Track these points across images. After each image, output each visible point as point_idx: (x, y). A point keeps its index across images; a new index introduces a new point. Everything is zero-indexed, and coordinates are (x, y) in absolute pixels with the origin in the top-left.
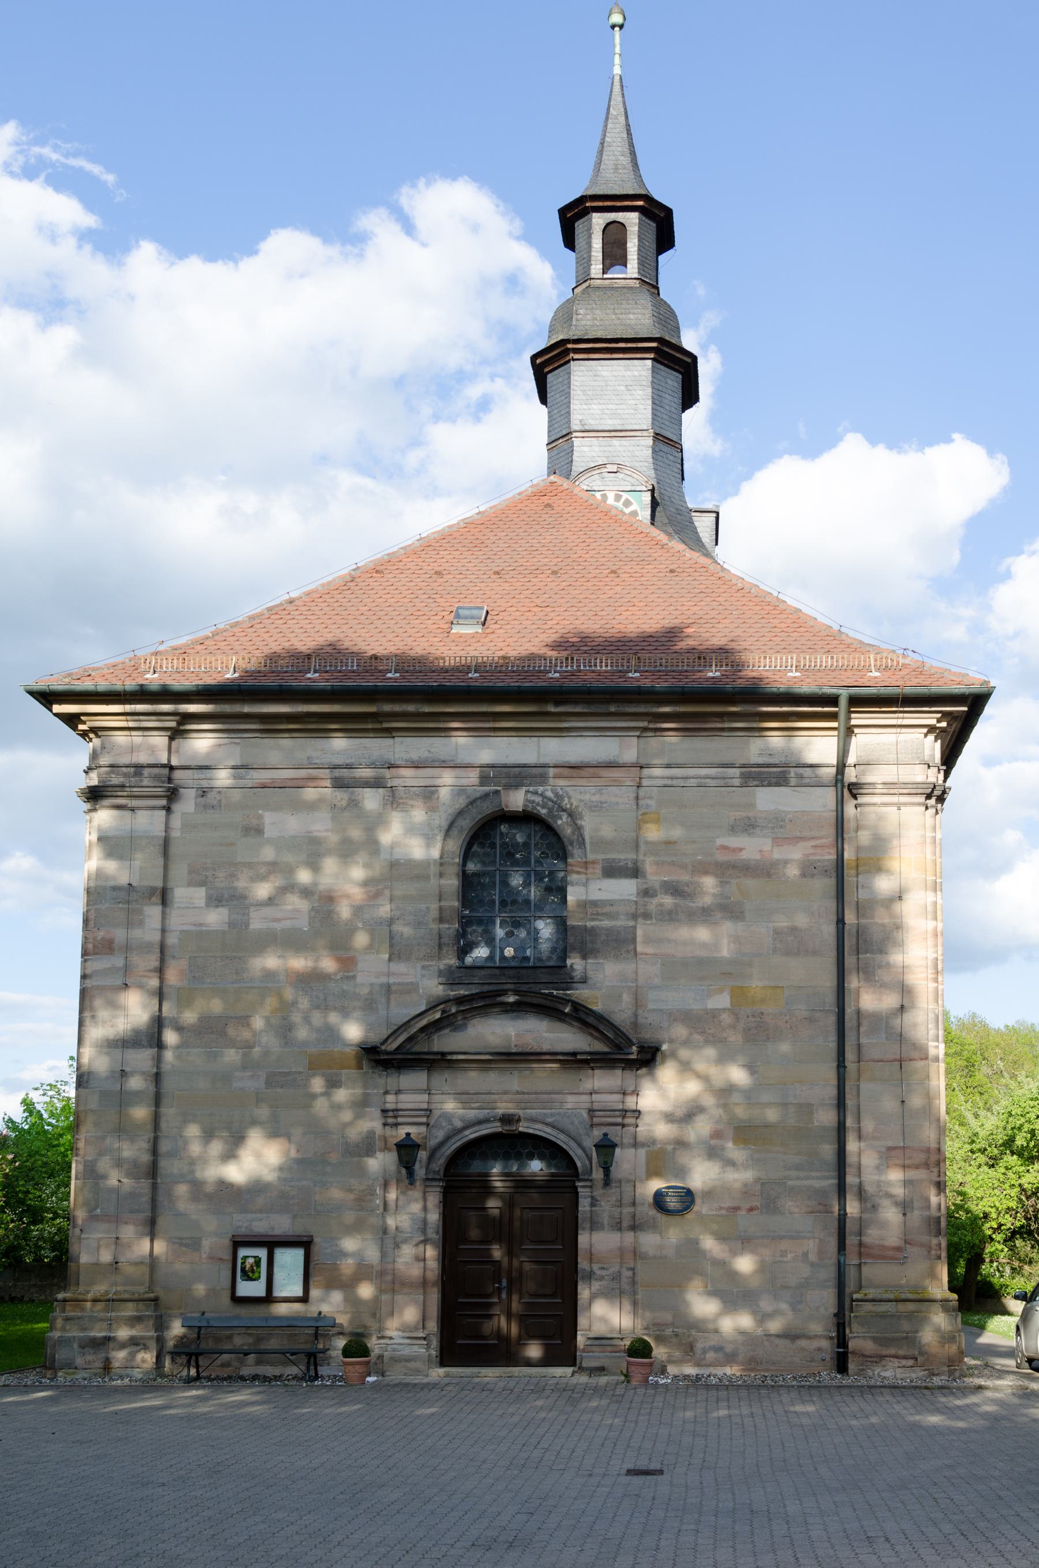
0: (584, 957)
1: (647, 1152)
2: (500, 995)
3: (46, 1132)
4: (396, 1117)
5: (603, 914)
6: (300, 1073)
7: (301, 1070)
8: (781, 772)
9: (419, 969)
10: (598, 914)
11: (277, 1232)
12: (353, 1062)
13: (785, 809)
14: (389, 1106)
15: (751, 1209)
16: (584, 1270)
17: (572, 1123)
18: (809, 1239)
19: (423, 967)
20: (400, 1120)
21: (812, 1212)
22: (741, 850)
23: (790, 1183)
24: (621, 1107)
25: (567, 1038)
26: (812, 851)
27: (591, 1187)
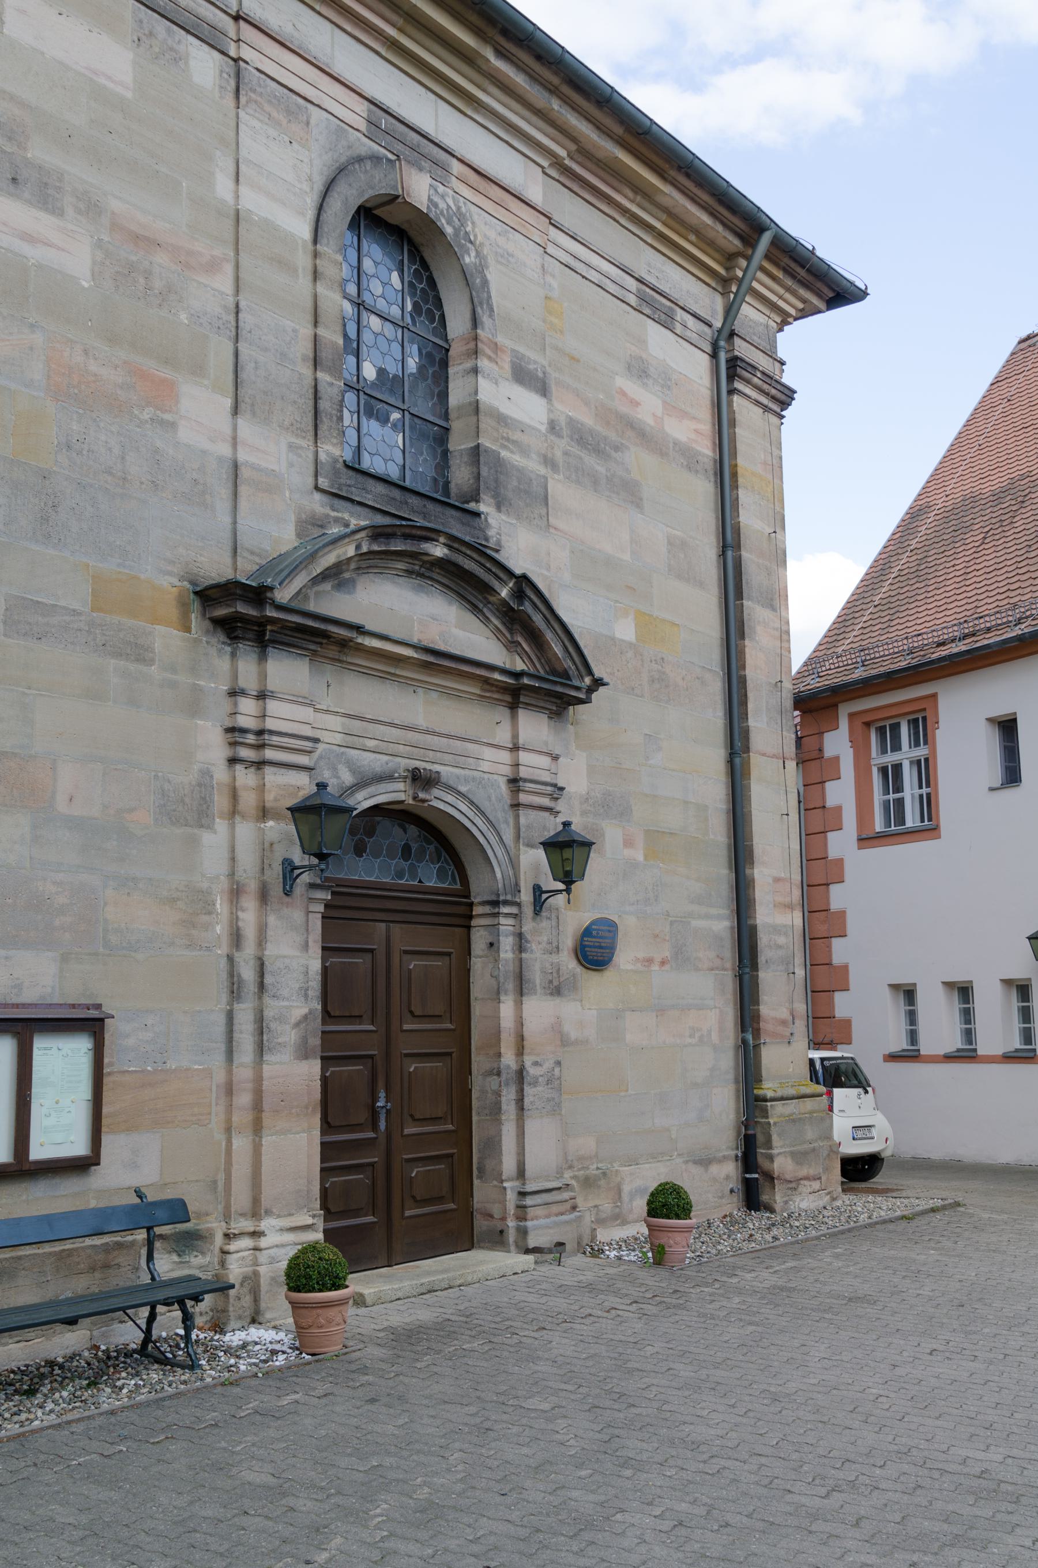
0: (499, 508)
1: (220, 818)
2: (427, 539)
3: (416, 305)
4: (260, 747)
5: (514, 442)
6: (75, 612)
7: (76, 606)
8: (669, 308)
9: (284, 447)
10: (508, 439)
11: (28, 996)
12: (173, 612)
13: (675, 367)
14: (243, 722)
15: (663, 963)
16: (508, 1067)
17: (489, 798)
18: (711, 1009)
19: (291, 447)
20: (269, 754)
21: (712, 970)
22: (638, 404)
23: (696, 923)
24: (546, 777)
25: (476, 639)
26: (693, 436)
27: (515, 916)
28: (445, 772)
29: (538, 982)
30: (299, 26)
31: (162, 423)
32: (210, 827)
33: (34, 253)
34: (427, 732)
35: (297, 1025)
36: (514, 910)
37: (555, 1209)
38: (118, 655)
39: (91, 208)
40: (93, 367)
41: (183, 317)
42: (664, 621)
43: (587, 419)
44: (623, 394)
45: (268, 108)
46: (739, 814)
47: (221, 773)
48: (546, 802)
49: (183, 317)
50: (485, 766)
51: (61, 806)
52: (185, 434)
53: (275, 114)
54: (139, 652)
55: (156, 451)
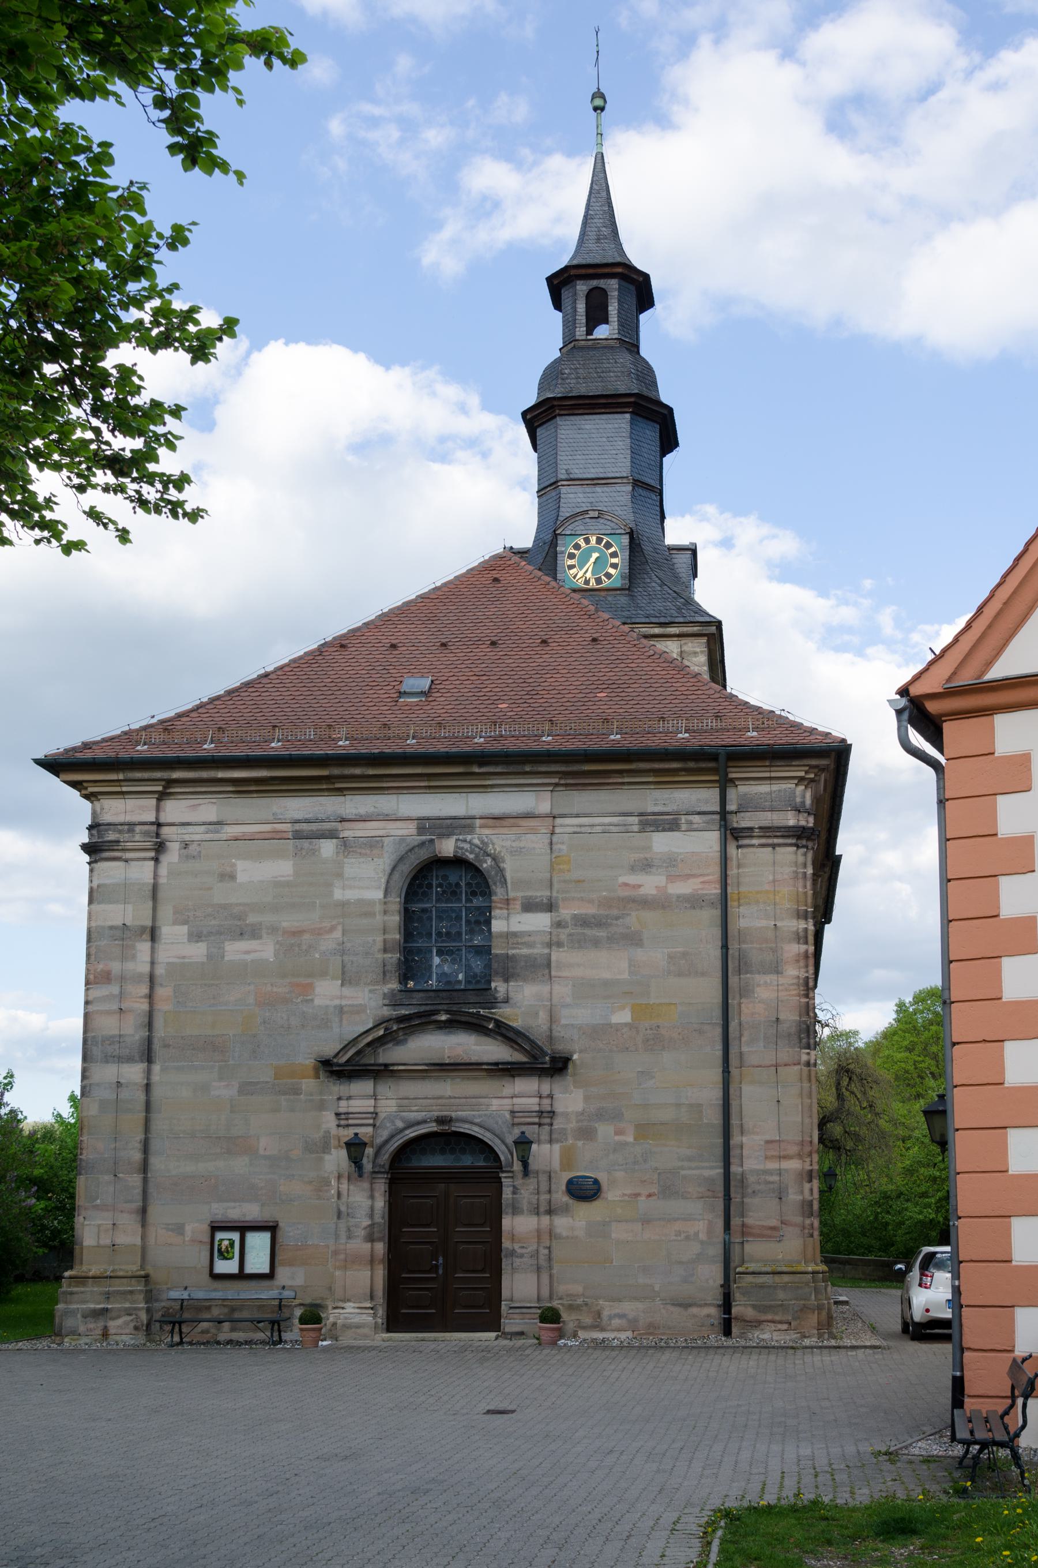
2: (434, 1015)
10: (518, 943)
11: (248, 1218)
12: (312, 1073)
15: (650, 1195)
17: (497, 1123)
19: (370, 991)
22: (640, 886)
23: (683, 1172)
28: (453, 1115)
29: (525, 1208)
30: (377, 805)
31: (307, 1001)
32: (329, 1153)
33: (249, 957)
34: (450, 1097)
35: (365, 1228)
36: (510, 1175)
37: (528, 1316)
38: (285, 1094)
39: (273, 930)
40: (275, 989)
41: (317, 956)
42: (661, 1004)
43: (590, 910)
44: (626, 885)
45: (359, 851)
46: (734, 1104)
47: (334, 1131)
48: (536, 1120)
49: (317, 956)
50: (494, 1108)
51: (261, 1152)
52: (317, 1002)
53: (363, 851)
54: (296, 1091)
55: (304, 1012)
